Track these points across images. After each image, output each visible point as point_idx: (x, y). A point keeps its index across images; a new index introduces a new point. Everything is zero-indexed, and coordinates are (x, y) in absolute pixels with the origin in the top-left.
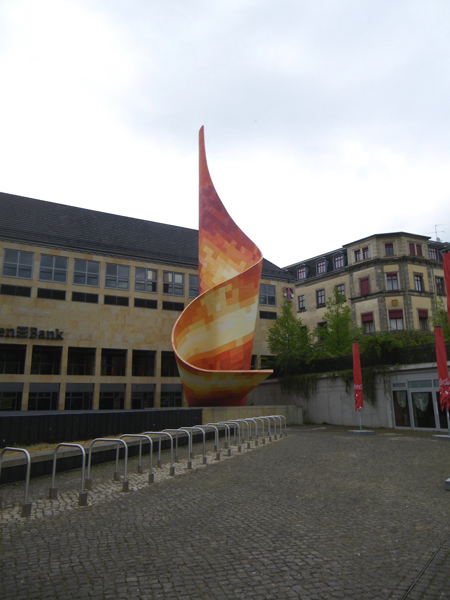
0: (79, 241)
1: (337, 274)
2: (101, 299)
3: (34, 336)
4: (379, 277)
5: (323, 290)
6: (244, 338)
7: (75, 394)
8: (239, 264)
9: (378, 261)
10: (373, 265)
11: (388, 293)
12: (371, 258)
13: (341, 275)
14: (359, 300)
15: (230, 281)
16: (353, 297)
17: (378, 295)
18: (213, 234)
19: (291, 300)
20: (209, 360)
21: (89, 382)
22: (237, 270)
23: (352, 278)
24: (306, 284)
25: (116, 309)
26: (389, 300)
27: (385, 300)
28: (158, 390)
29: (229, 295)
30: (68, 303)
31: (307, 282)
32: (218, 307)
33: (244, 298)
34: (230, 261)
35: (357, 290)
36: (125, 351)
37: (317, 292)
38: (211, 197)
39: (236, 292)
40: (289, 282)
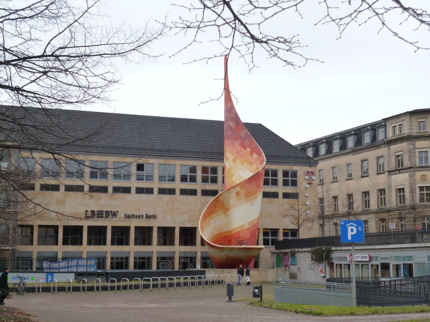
0: (139, 149)
1: (378, 146)
2: (156, 191)
3: (107, 216)
4: (411, 152)
5: (367, 160)
6: (250, 223)
7: (140, 258)
8: (252, 166)
9: (410, 137)
10: (406, 141)
11: (419, 168)
12: (404, 134)
13: (382, 146)
14: (394, 173)
15: (238, 185)
16: (390, 170)
17: (409, 170)
18: (233, 144)
19: (313, 182)
20: (225, 238)
21: (149, 250)
22: (251, 171)
23: (390, 151)
24: (354, 153)
25: (166, 197)
26: (418, 175)
27: (415, 175)
28: (199, 256)
29: (238, 194)
30: (133, 196)
31: (354, 151)
32: (231, 202)
33: (249, 195)
34: (246, 164)
35: (393, 164)
36: (173, 229)
37: (362, 161)
38: (232, 115)
39: (243, 192)
40: (311, 166)
